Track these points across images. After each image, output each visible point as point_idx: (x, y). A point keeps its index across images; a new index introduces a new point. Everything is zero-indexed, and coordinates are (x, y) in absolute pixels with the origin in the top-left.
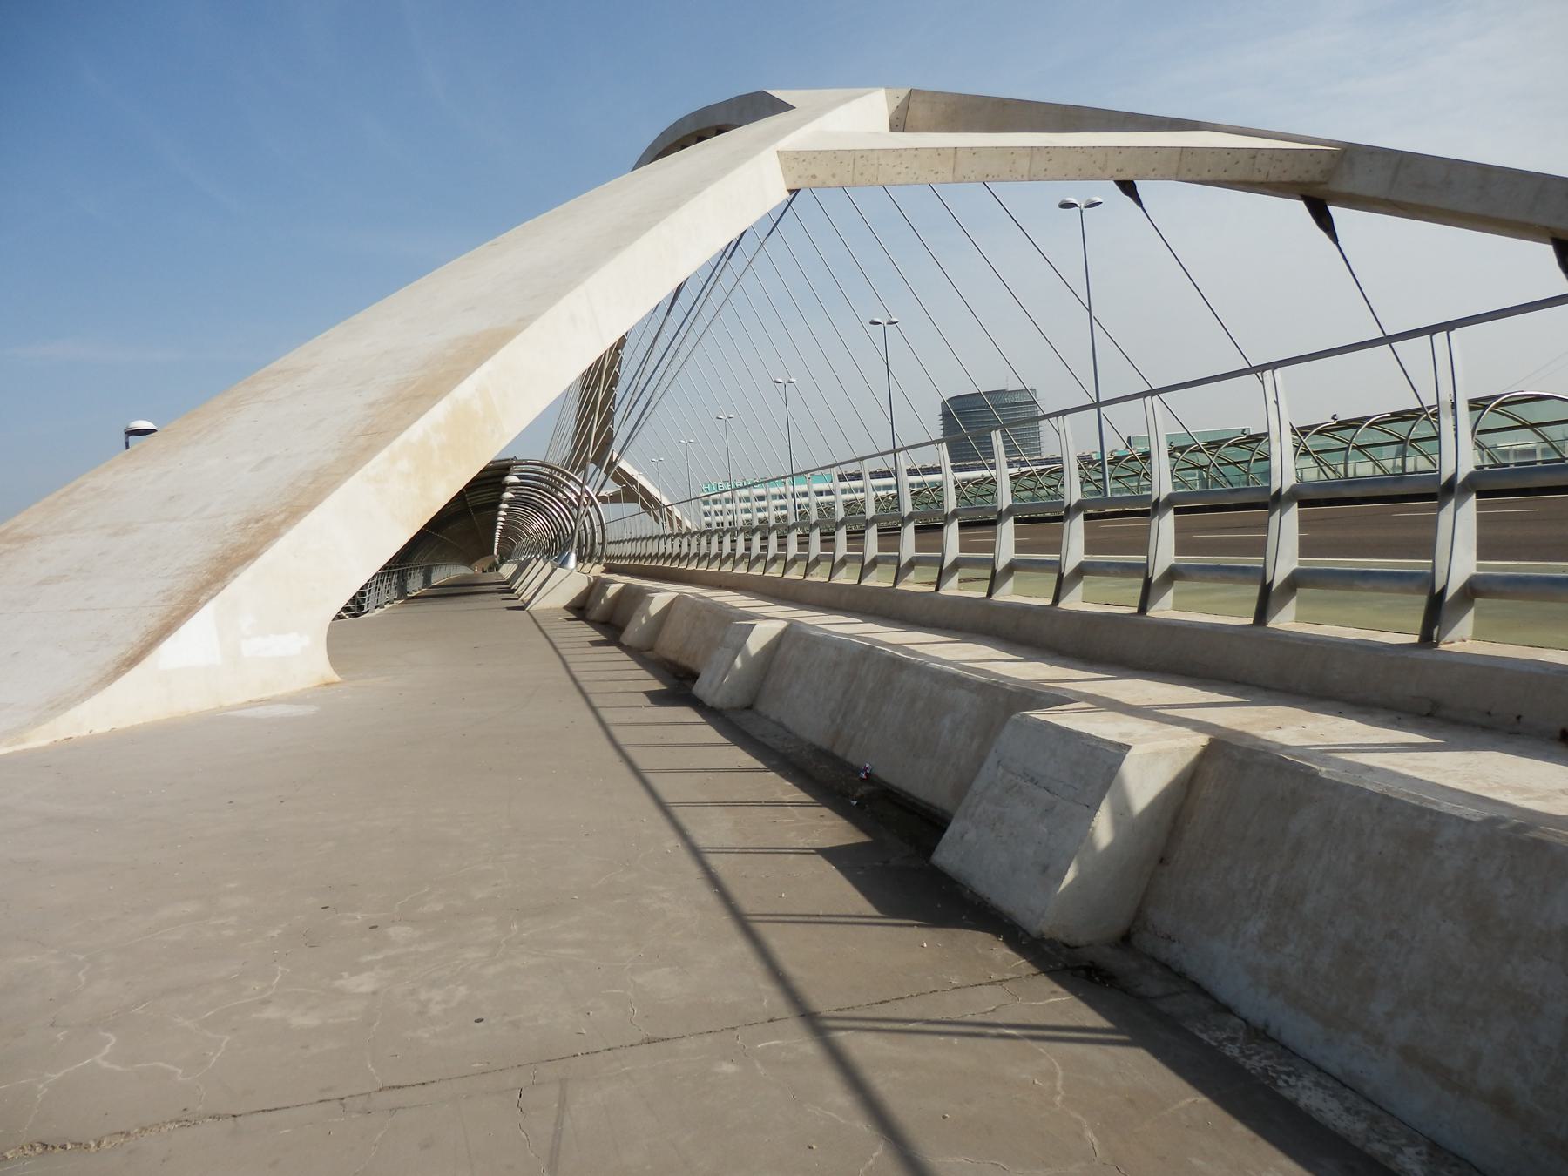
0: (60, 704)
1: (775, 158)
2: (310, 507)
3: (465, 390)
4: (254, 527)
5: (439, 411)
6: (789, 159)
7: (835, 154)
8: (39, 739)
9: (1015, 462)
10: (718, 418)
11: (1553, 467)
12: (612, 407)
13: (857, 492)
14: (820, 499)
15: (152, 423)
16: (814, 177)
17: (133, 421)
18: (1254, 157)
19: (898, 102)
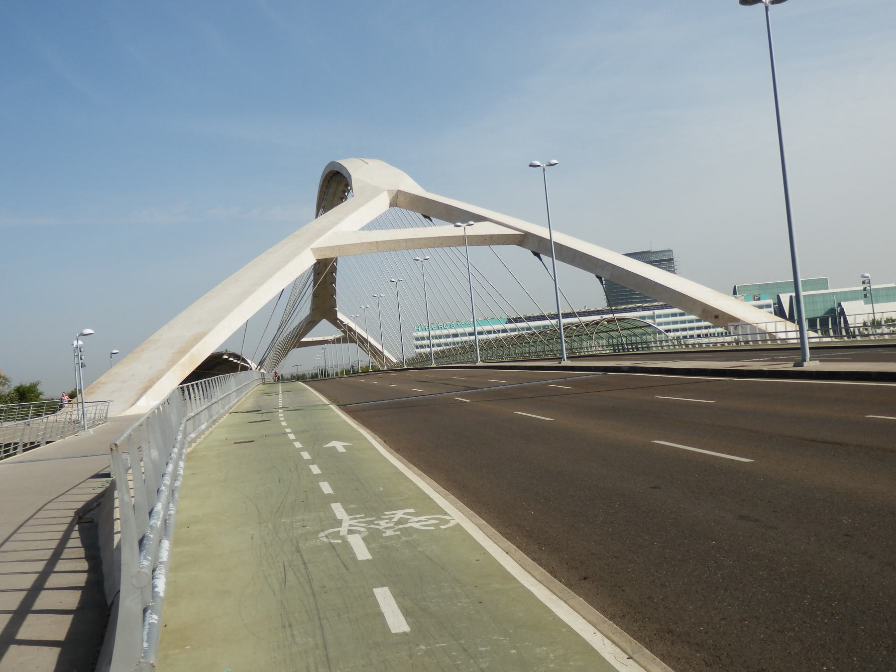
0: (124, 410)
1: (310, 251)
2: (161, 377)
3: (194, 350)
4: (151, 382)
5: (187, 356)
6: (314, 251)
7: (332, 247)
8: (123, 414)
9: (638, 307)
10: (391, 281)
11: (885, 334)
12: (335, 264)
13: (499, 333)
14: (481, 337)
15: (93, 330)
16: (325, 255)
17: (84, 329)
18: (491, 238)
19: (393, 195)
